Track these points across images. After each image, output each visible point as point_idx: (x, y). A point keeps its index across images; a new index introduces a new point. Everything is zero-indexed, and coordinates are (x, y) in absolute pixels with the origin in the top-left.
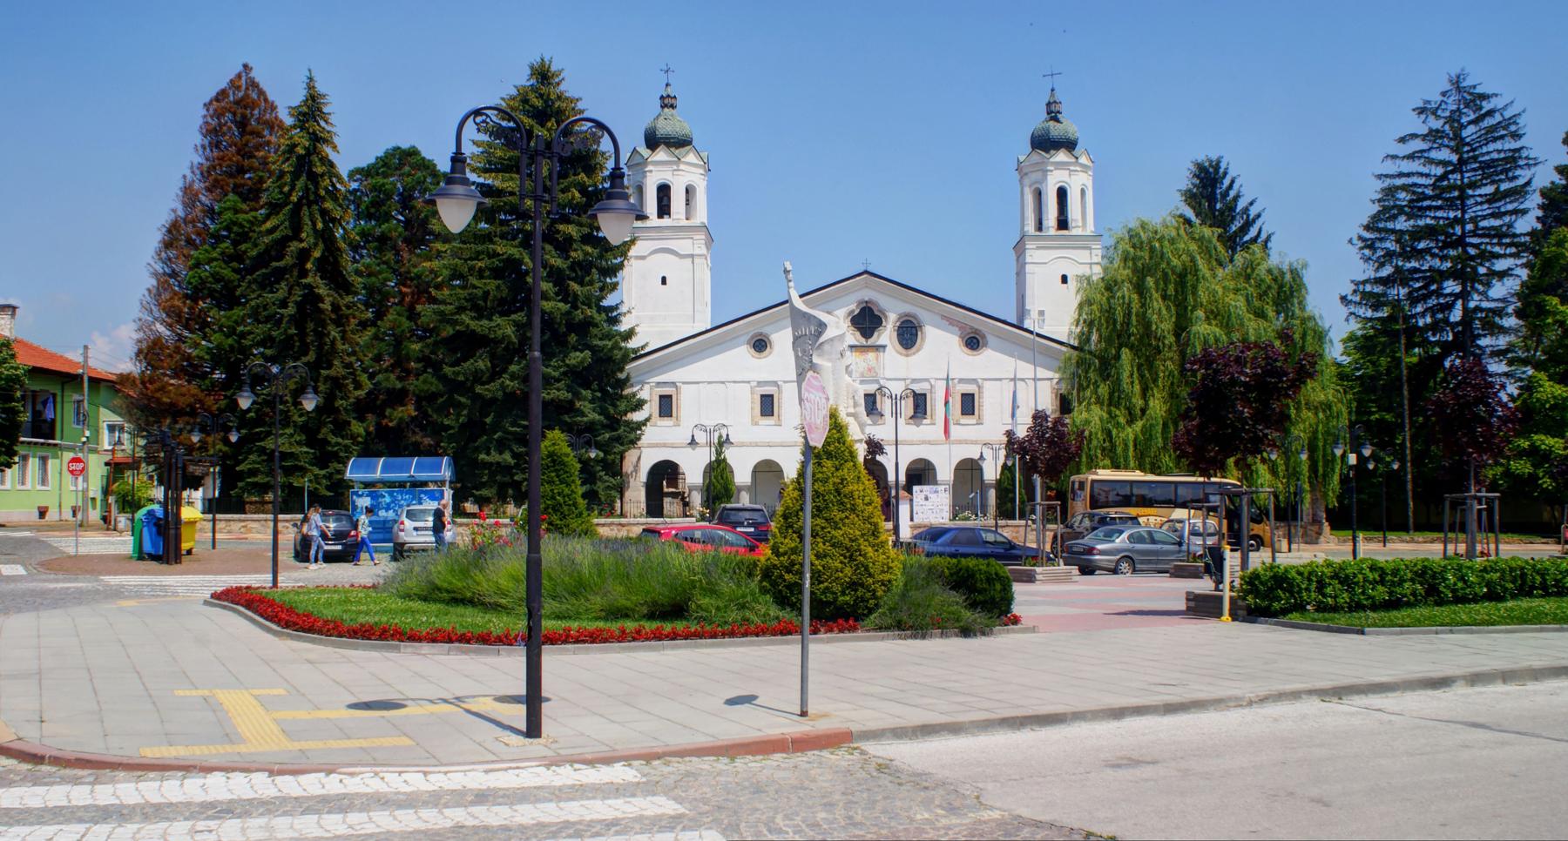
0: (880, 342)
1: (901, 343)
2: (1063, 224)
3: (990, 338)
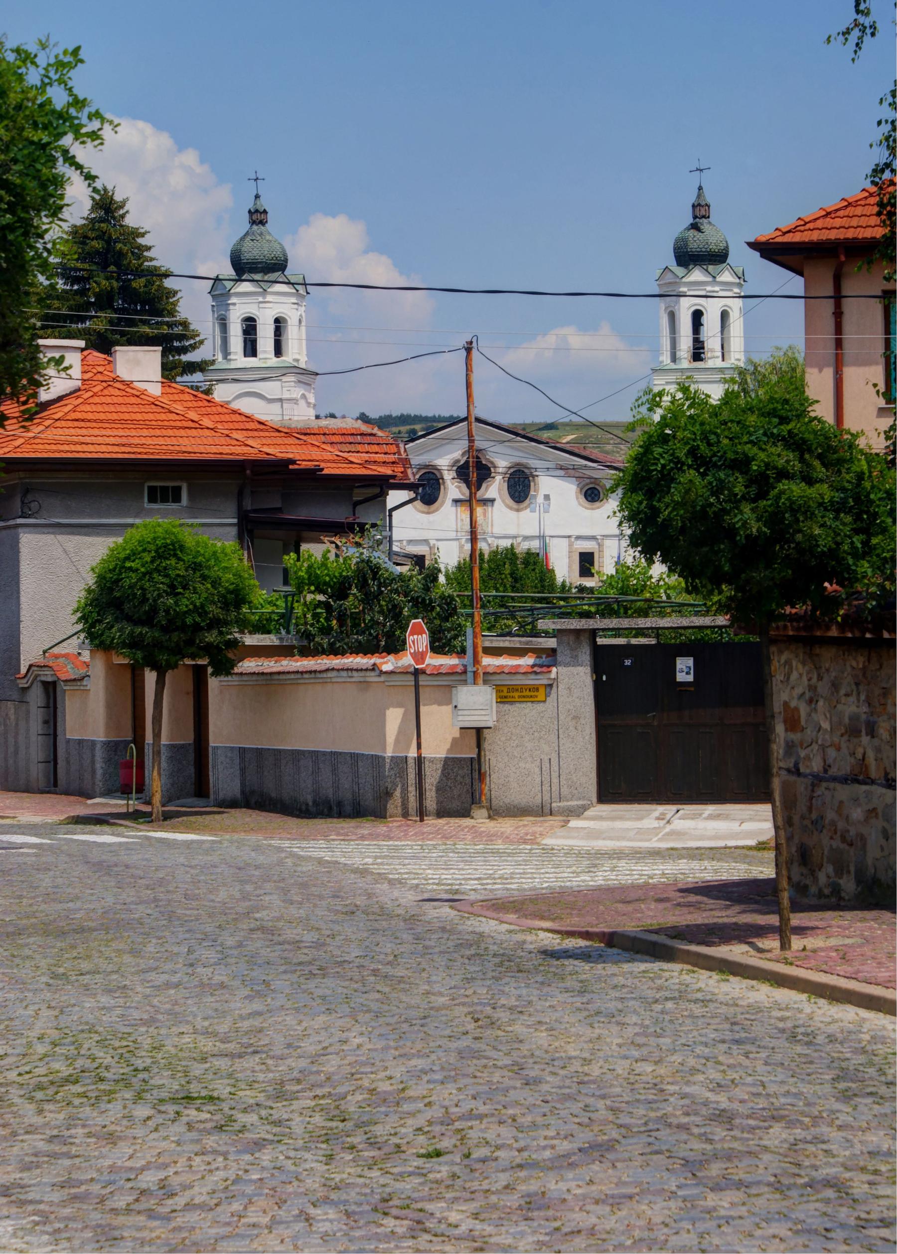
1: (512, 497)
2: (698, 354)
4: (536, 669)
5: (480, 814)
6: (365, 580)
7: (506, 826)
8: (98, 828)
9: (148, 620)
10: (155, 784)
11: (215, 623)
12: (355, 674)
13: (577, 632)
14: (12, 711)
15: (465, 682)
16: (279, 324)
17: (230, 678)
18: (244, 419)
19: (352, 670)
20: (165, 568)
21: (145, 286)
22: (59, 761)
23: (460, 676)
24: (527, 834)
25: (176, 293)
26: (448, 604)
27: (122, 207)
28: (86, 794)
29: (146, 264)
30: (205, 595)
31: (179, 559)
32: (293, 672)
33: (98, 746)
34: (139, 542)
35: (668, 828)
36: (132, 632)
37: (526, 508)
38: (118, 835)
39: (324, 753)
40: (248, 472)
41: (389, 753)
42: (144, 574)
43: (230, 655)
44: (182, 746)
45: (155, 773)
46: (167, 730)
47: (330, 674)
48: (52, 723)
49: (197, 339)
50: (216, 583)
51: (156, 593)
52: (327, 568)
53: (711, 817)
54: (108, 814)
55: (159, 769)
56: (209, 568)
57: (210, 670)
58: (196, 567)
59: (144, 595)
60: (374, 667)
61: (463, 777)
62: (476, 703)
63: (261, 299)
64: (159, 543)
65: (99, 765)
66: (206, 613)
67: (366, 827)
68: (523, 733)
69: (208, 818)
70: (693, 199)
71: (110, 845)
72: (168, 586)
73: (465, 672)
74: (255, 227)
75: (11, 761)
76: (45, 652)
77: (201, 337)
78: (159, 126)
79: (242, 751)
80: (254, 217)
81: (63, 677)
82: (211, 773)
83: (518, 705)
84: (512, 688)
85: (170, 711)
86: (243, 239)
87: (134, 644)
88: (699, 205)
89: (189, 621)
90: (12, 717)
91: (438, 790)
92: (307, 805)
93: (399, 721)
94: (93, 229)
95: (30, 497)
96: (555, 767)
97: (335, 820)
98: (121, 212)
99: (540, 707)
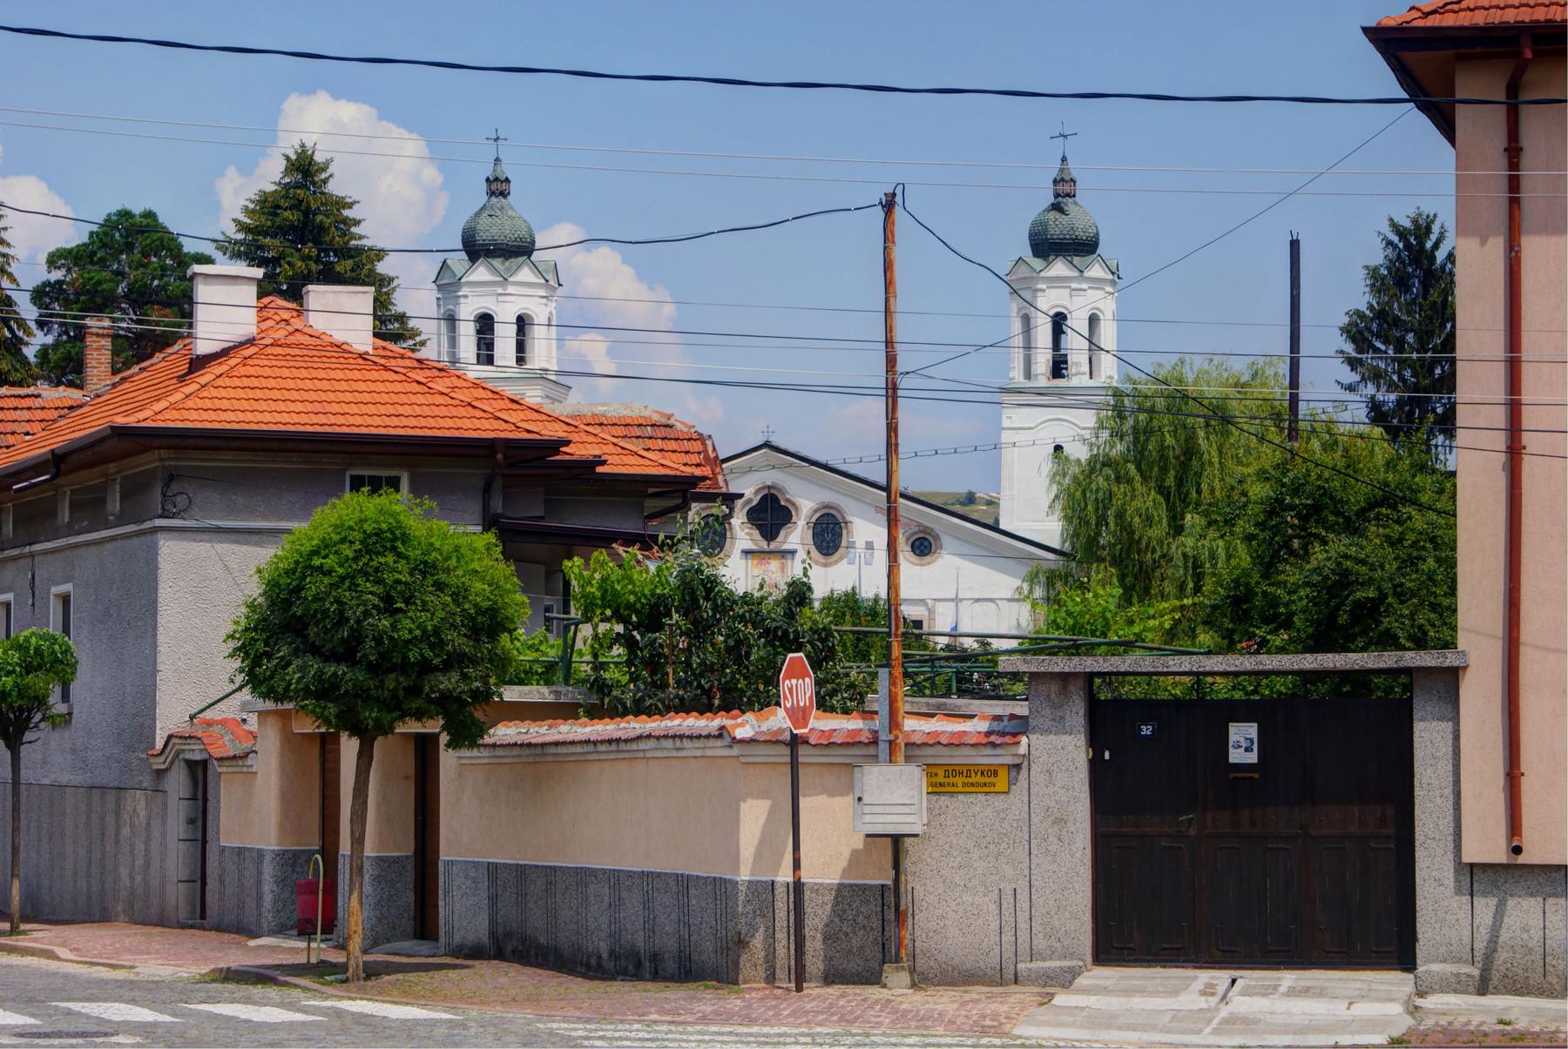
0: (786, 547)
2: (1059, 367)
3: (945, 539)
4: (993, 738)
5: (898, 979)
6: (695, 600)
7: (944, 1001)
8: (257, 991)
9: (347, 653)
10: (353, 921)
11: (456, 661)
12: (687, 743)
13: (1064, 678)
14: (143, 803)
15: (875, 758)
16: (522, 323)
17: (475, 752)
18: (490, 395)
19: (681, 737)
20: (377, 570)
21: (352, 270)
22: (208, 881)
23: (869, 747)
24: (984, 1017)
25: (391, 280)
26: (823, 641)
27: (324, 170)
28: (246, 930)
29: (353, 242)
30: (440, 614)
31: (400, 555)
32: (580, 742)
33: (268, 859)
34: (336, 526)
35: (1224, 1012)
36: (320, 672)
37: (841, 558)
38: (291, 1006)
39: (630, 874)
40: (499, 456)
41: (744, 875)
42: (343, 578)
43: (478, 715)
44: (396, 860)
45: (355, 902)
46: (374, 834)
47: (643, 745)
48: (200, 823)
49: (418, 339)
50: (459, 595)
51: (361, 608)
52: (631, 582)
53: (1292, 993)
54: (277, 967)
55: (361, 893)
56: (447, 571)
57: (444, 738)
58: (425, 568)
59: (341, 613)
60: (721, 733)
61: (868, 918)
62: (894, 796)
63: (500, 290)
64: (368, 527)
65: (269, 888)
66: (442, 643)
67: (706, 999)
68: (970, 844)
69: (439, 975)
70: (1054, 174)
71: (273, 1027)
72: (381, 599)
73: (874, 742)
74: (494, 199)
75: (139, 879)
76: (192, 717)
77: (423, 337)
78: (372, 105)
79: (493, 869)
80: (494, 187)
81: (217, 753)
82: (441, 903)
83: (961, 797)
84: (953, 771)
85: (379, 805)
86: (478, 214)
87: (324, 691)
88: (1063, 180)
89: (413, 655)
90: (143, 814)
91: (826, 938)
92: (600, 957)
93: (762, 821)
94: (286, 197)
95: (175, 487)
96: (1023, 903)
97: (650, 985)
98: (323, 176)
99: (999, 802)
